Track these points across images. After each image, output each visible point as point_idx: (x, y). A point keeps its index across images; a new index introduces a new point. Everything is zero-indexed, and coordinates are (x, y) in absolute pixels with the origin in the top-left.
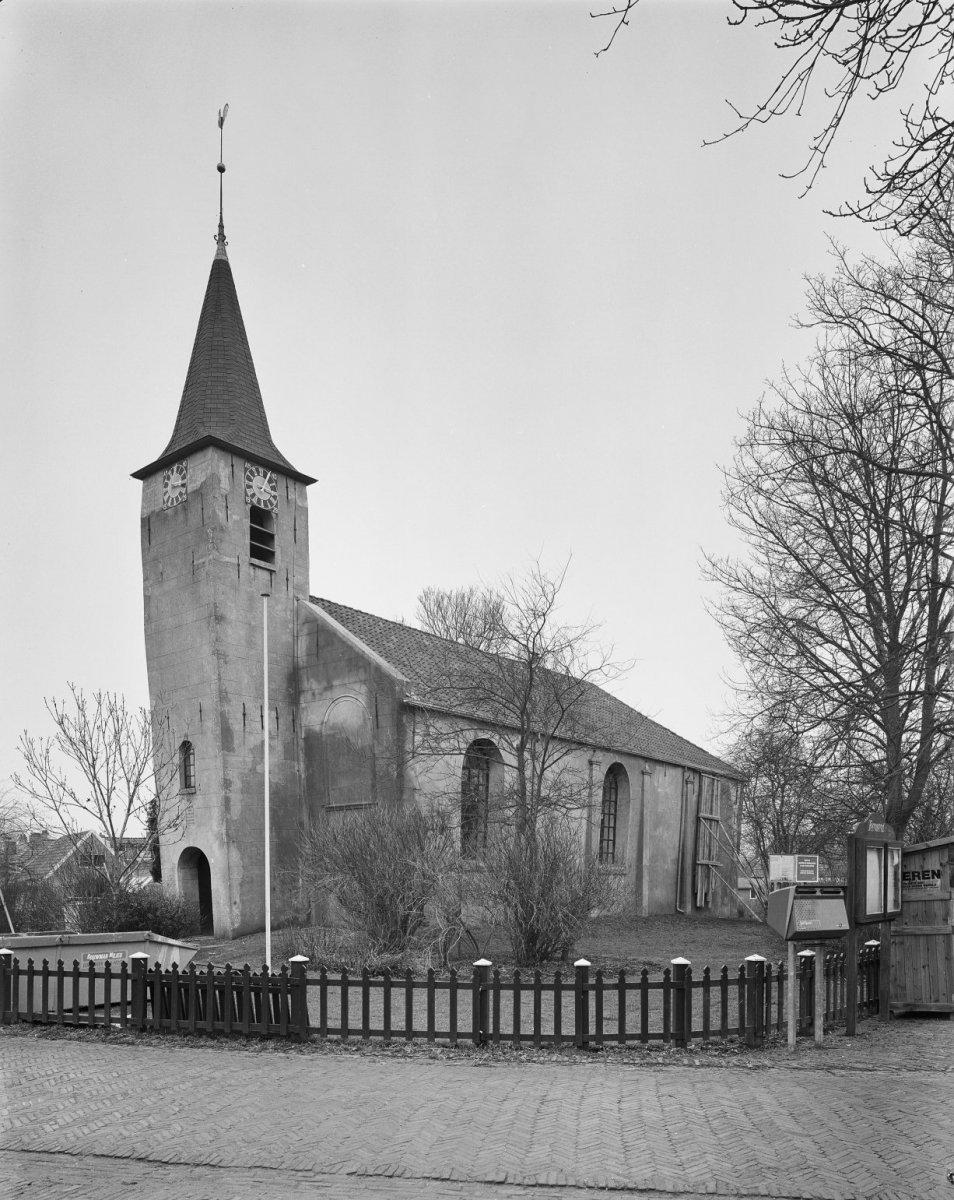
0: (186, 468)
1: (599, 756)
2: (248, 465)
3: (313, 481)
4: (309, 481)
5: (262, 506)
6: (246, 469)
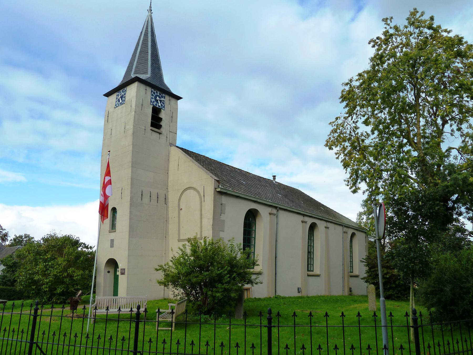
0: (126, 90)
1: (306, 219)
2: (153, 90)
3: (181, 98)
4: (178, 98)
5: (157, 106)
6: (152, 91)
